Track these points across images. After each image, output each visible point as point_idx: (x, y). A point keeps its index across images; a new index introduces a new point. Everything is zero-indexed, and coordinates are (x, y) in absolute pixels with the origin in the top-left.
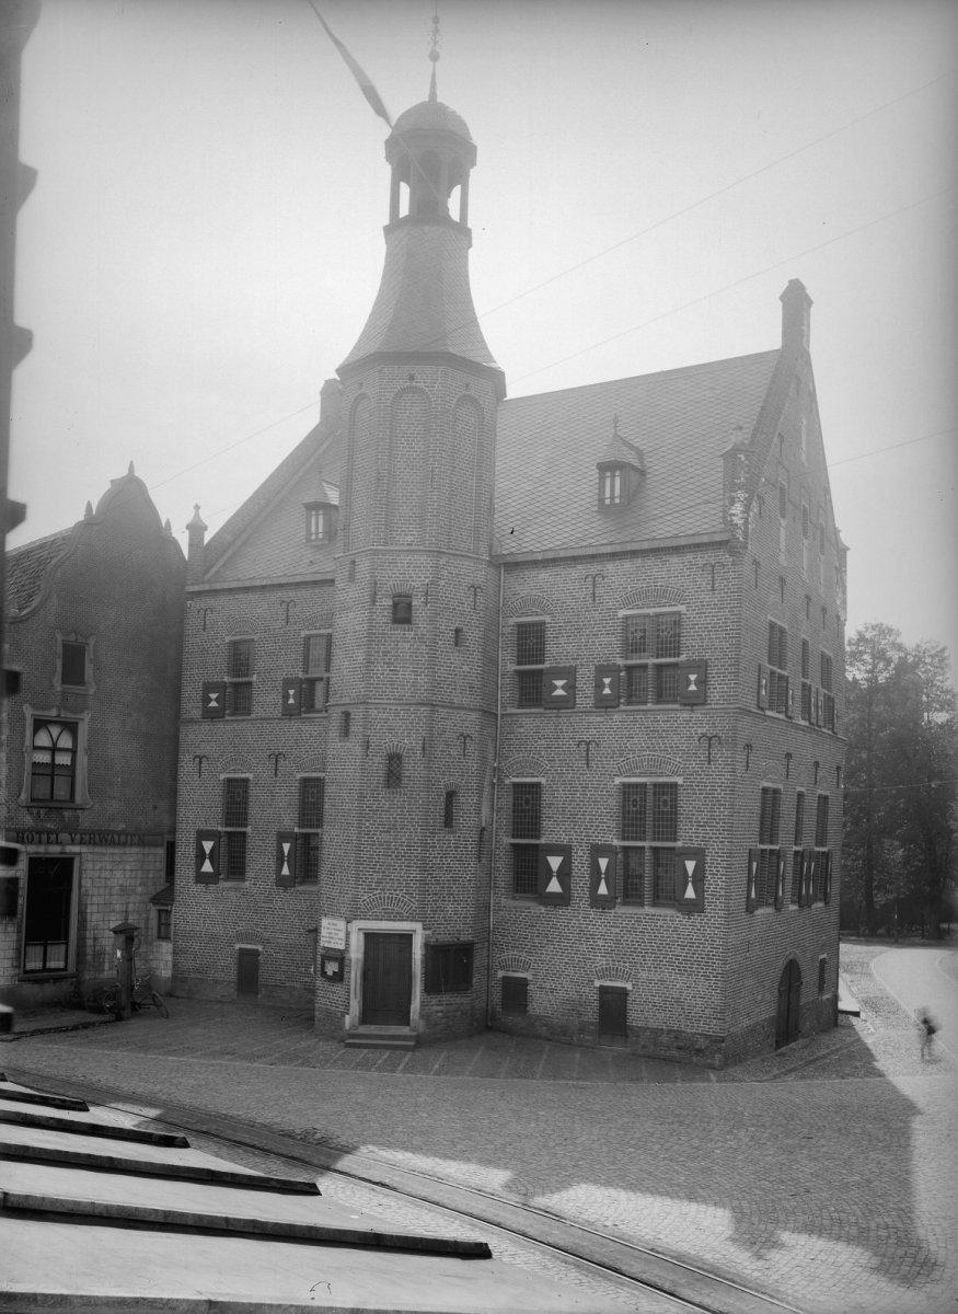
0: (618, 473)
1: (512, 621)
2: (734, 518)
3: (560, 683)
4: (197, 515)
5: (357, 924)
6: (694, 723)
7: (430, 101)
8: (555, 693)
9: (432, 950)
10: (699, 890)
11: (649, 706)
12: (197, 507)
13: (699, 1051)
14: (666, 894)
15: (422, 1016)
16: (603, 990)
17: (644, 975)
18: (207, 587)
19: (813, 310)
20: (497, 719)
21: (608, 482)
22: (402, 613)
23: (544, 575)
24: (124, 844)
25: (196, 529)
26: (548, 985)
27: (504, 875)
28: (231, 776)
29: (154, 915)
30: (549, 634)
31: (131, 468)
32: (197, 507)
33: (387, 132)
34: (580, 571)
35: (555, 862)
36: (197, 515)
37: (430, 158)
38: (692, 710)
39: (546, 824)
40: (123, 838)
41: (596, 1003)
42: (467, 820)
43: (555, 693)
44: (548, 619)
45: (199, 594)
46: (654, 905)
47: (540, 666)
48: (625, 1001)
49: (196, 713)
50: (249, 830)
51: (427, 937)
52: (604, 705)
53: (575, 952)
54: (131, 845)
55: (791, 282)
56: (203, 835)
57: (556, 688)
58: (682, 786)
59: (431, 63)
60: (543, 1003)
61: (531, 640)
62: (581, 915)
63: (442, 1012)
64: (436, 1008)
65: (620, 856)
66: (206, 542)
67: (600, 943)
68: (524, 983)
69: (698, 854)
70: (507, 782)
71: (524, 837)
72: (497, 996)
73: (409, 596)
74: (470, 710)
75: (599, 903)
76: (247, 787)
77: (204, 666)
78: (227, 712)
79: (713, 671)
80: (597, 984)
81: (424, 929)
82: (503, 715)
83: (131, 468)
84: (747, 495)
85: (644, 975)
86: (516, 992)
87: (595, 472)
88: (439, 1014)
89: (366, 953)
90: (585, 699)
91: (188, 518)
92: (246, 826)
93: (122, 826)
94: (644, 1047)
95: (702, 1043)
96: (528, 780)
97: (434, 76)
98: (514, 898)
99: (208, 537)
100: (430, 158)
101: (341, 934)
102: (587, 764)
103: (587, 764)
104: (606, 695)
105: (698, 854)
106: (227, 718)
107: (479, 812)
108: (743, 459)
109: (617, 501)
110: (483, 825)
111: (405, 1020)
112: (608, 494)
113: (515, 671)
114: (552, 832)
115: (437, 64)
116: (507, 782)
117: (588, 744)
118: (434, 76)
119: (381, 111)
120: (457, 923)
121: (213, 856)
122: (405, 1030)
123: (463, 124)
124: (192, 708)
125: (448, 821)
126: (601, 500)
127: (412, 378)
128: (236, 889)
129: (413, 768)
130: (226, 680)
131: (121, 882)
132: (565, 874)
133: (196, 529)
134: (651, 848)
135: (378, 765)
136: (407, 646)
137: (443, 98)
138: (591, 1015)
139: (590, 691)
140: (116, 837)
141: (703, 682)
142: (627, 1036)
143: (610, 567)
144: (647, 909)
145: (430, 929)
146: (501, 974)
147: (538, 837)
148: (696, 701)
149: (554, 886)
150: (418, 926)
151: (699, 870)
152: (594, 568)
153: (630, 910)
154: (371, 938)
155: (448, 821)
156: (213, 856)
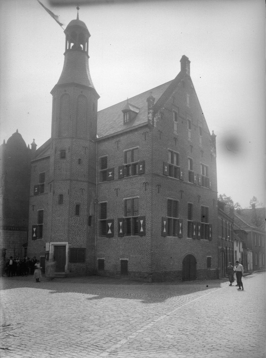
0: (128, 113)
1: (100, 157)
2: (149, 118)
3: (110, 173)
4: (34, 142)
5: (52, 243)
6: (142, 179)
7: (77, 19)
8: (109, 176)
9: (71, 250)
10: (144, 229)
11: (131, 176)
12: (34, 140)
13: (145, 278)
14: (136, 231)
15: (68, 269)
16: (122, 261)
17: (131, 256)
18: (35, 160)
19: (191, 64)
20: (96, 185)
21: (126, 116)
22: (63, 156)
23: (106, 143)
24: (14, 230)
25: (34, 145)
26: (109, 261)
27: (98, 231)
28: (40, 210)
29: (23, 249)
30: (108, 160)
31: (17, 131)
32: (34, 140)
33: (64, 31)
34: (114, 141)
35: (110, 224)
36: (34, 142)
37: (77, 35)
38: (141, 176)
39: (108, 214)
40: (13, 228)
41: (120, 265)
42: (83, 212)
43: (109, 176)
44: (107, 155)
45: (34, 162)
46: (134, 235)
47: (106, 169)
48: (127, 264)
49: (33, 194)
50: (43, 224)
51: (70, 246)
52: (121, 178)
53: (115, 250)
54: (16, 230)
55: (182, 56)
56: (34, 227)
57: (109, 174)
58: (139, 198)
59: (77, 10)
60: (108, 266)
61: (104, 162)
62: (115, 240)
63: (75, 268)
64: (73, 267)
65: (125, 221)
66: (37, 149)
67: (121, 247)
68: (103, 261)
69: (144, 218)
70: (99, 203)
71: (103, 219)
72: (97, 265)
73: (65, 151)
74: (84, 182)
75: (121, 235)
76: (43, 212)
77: (35, 181)
78: (39, 193)
79: (146, 164)
80: (120, 259)
81: (69, 244)
82: (98, 184)
83: (17, 131)
84: (153, 111)
85: (131, 256)
86: (101, 263)
87: (123, 114)
88: (75, 269)
89: (55, 251)
90: (116, 177)
91: (32, 142)
92: (42, 223)
93: (13, 225)
94: (132, 277)
95: (146, 275)
96: (103, 202)
97: (78, 13)
98: (101, 237)
99: (37, 148)
100: (77, 35)
101: (50, 247)
102: (117, 195)
103: (117, 195)
104: (121, 175)
105: (144, 218)
106: (39, 194)
107: (88, 211)
108: (152, 101)
109: (128, 121)
110: (91, 215)
111: (64, 271)
112: (126, 120)
113: (101, 171)
114: (110, 216)
115: (79, 10)
116: (99, 203)
117: (117, 189)
118: (78, 13)
119: (61, 25)
120: (81, 242)
121: (36, 232)
122: (64, 273)
123: (84, 24)
124: (32, 193)
125: (77, 213)
126: (124, 121)
128: (41, 241)
129: (66, 199)
130: (39, 184)
131: (13, 240)
132: (112, 228)
134: (132, 218)
135: (57, 198)
136: (64, 164)
137: (80, 19)
138: (119, 269)
139: (117, 175)
140: (11, 228)
141: (144, 167)
142: (128, 275)
143: (121, 138)
144: (132, 236)
145: (70, 244)
146: (98, 259)
147: (106, 218)
148: (142, 173)
149: (110, 232)
150: (67, 243)
151: (144, 222)
152: (118, 139)
153: (128, 237)
154: (56, 247)
155: (77, 213)
156: (36, 232)
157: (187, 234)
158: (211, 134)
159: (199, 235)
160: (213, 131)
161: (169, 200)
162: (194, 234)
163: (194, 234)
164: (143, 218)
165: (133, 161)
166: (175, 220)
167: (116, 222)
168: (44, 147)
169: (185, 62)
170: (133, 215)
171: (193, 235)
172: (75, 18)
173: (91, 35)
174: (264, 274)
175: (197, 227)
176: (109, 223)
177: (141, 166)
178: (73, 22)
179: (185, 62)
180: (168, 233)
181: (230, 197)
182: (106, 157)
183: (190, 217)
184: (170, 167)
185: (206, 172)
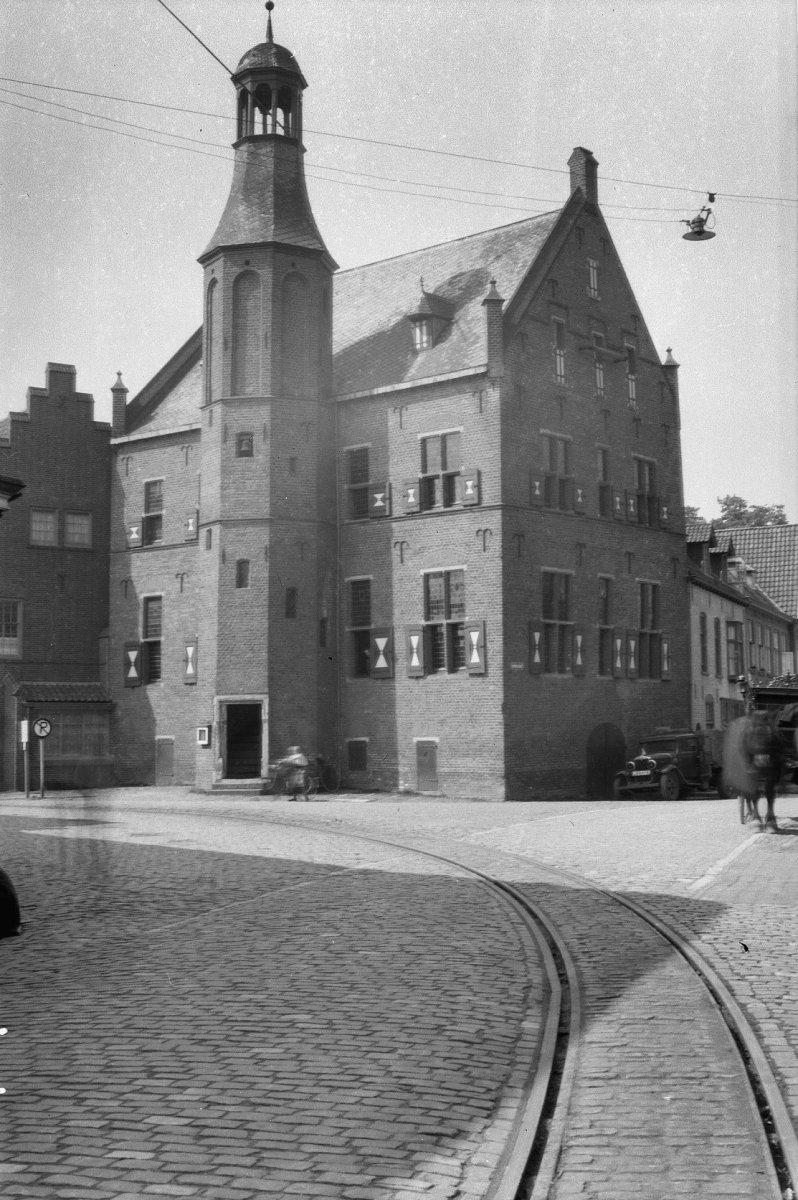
0: (424, 323)
3: (379, 496)
25: (119, 391)
27: (348, 661)
97: (270, 21)
99: (129, 398)
116: (347, 580)
118: (270, 21)
127: (247, 263)
133: (119, 391)
134: (448, 625)
157: (597, 665)
158: (663, 359)
159: (632, 665)
160: (669, 351)
161: (546, 573)
162: (618, 665)
163: (618, 665)
164: (477, 626)
165: (444, 466)
166: (562, 627)
167: (399, 636)
168: (221, 761)
169: (585, 165)
170: (449, 618)
171: (613, 668)
172: (264, 40)
173: (308, 81)
174: (795, 800)
175: (626, 645)
176: (382, 666)
177: (470, 483)
178: (260, 49)
179: (585, 165)
180: (547, 667)
181: (686, 237)
182: (365, 451)
183: (605, 616)
184: (548, 481)
185: (653, 601)
